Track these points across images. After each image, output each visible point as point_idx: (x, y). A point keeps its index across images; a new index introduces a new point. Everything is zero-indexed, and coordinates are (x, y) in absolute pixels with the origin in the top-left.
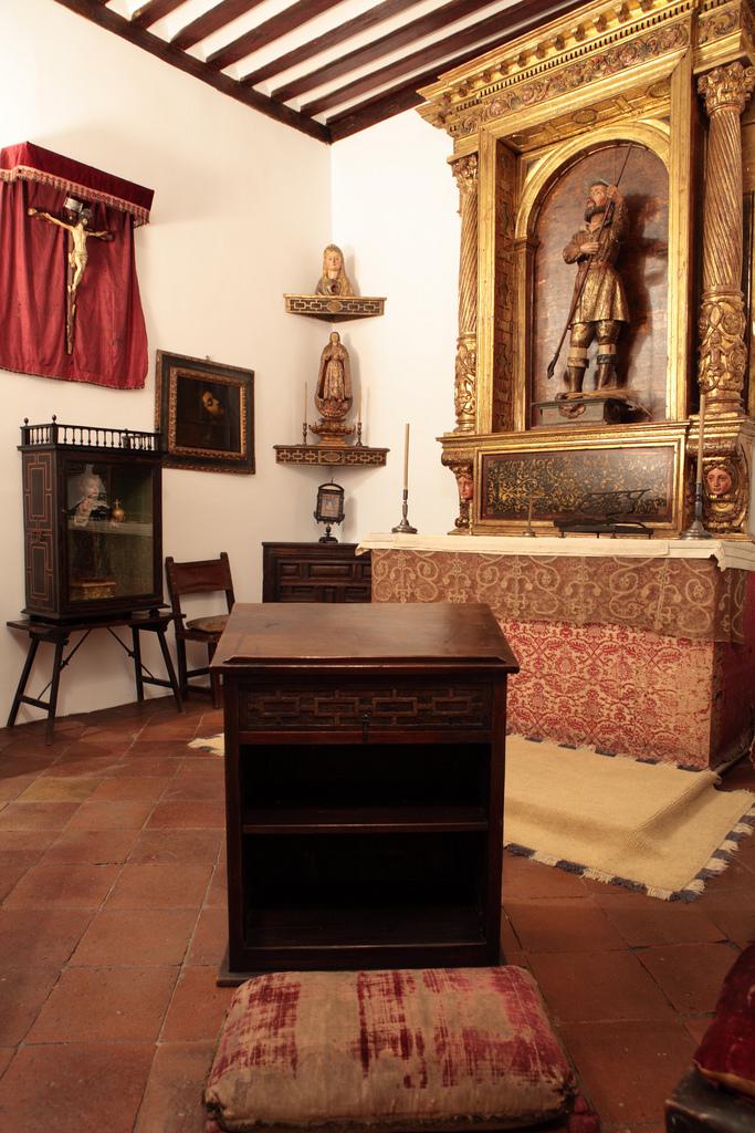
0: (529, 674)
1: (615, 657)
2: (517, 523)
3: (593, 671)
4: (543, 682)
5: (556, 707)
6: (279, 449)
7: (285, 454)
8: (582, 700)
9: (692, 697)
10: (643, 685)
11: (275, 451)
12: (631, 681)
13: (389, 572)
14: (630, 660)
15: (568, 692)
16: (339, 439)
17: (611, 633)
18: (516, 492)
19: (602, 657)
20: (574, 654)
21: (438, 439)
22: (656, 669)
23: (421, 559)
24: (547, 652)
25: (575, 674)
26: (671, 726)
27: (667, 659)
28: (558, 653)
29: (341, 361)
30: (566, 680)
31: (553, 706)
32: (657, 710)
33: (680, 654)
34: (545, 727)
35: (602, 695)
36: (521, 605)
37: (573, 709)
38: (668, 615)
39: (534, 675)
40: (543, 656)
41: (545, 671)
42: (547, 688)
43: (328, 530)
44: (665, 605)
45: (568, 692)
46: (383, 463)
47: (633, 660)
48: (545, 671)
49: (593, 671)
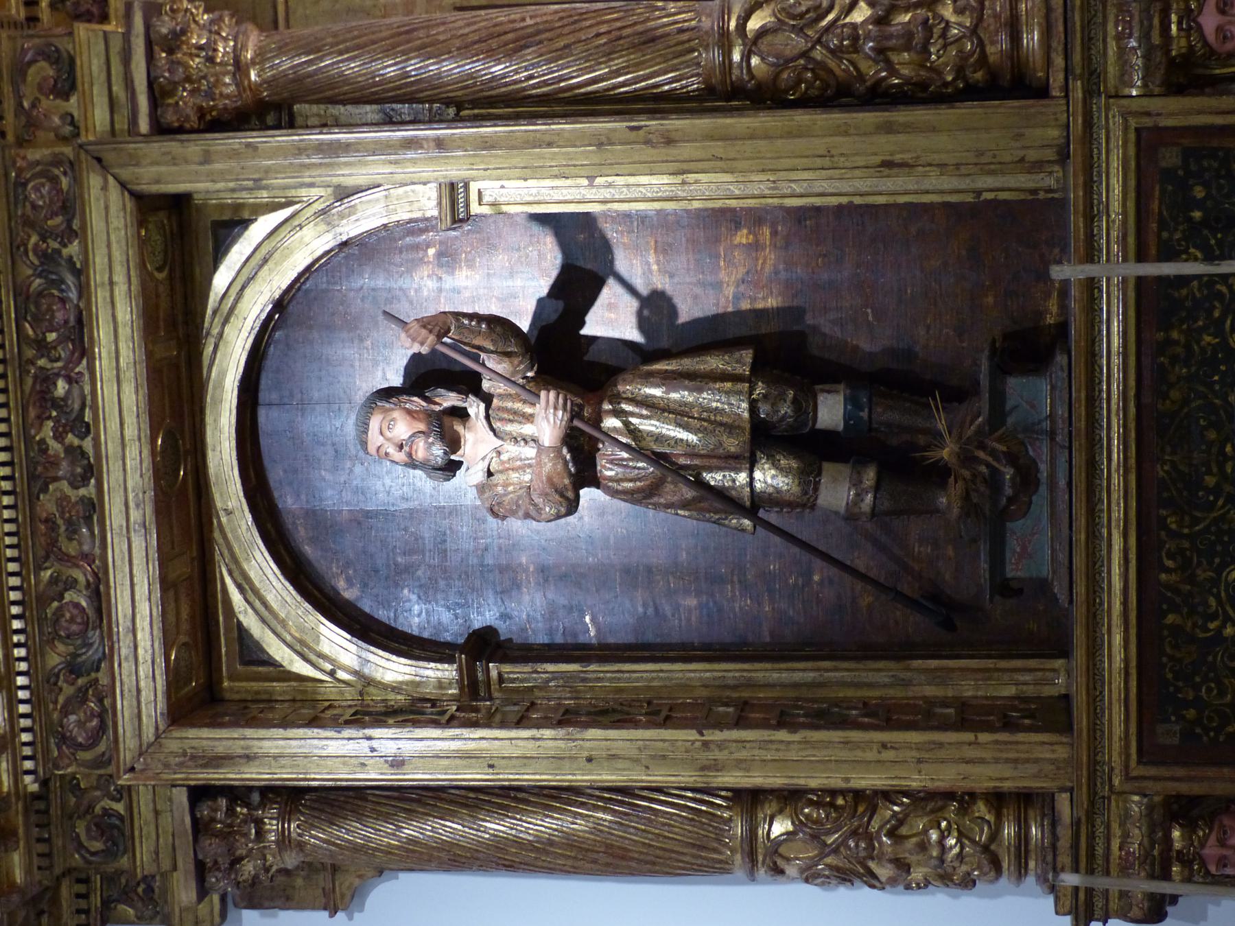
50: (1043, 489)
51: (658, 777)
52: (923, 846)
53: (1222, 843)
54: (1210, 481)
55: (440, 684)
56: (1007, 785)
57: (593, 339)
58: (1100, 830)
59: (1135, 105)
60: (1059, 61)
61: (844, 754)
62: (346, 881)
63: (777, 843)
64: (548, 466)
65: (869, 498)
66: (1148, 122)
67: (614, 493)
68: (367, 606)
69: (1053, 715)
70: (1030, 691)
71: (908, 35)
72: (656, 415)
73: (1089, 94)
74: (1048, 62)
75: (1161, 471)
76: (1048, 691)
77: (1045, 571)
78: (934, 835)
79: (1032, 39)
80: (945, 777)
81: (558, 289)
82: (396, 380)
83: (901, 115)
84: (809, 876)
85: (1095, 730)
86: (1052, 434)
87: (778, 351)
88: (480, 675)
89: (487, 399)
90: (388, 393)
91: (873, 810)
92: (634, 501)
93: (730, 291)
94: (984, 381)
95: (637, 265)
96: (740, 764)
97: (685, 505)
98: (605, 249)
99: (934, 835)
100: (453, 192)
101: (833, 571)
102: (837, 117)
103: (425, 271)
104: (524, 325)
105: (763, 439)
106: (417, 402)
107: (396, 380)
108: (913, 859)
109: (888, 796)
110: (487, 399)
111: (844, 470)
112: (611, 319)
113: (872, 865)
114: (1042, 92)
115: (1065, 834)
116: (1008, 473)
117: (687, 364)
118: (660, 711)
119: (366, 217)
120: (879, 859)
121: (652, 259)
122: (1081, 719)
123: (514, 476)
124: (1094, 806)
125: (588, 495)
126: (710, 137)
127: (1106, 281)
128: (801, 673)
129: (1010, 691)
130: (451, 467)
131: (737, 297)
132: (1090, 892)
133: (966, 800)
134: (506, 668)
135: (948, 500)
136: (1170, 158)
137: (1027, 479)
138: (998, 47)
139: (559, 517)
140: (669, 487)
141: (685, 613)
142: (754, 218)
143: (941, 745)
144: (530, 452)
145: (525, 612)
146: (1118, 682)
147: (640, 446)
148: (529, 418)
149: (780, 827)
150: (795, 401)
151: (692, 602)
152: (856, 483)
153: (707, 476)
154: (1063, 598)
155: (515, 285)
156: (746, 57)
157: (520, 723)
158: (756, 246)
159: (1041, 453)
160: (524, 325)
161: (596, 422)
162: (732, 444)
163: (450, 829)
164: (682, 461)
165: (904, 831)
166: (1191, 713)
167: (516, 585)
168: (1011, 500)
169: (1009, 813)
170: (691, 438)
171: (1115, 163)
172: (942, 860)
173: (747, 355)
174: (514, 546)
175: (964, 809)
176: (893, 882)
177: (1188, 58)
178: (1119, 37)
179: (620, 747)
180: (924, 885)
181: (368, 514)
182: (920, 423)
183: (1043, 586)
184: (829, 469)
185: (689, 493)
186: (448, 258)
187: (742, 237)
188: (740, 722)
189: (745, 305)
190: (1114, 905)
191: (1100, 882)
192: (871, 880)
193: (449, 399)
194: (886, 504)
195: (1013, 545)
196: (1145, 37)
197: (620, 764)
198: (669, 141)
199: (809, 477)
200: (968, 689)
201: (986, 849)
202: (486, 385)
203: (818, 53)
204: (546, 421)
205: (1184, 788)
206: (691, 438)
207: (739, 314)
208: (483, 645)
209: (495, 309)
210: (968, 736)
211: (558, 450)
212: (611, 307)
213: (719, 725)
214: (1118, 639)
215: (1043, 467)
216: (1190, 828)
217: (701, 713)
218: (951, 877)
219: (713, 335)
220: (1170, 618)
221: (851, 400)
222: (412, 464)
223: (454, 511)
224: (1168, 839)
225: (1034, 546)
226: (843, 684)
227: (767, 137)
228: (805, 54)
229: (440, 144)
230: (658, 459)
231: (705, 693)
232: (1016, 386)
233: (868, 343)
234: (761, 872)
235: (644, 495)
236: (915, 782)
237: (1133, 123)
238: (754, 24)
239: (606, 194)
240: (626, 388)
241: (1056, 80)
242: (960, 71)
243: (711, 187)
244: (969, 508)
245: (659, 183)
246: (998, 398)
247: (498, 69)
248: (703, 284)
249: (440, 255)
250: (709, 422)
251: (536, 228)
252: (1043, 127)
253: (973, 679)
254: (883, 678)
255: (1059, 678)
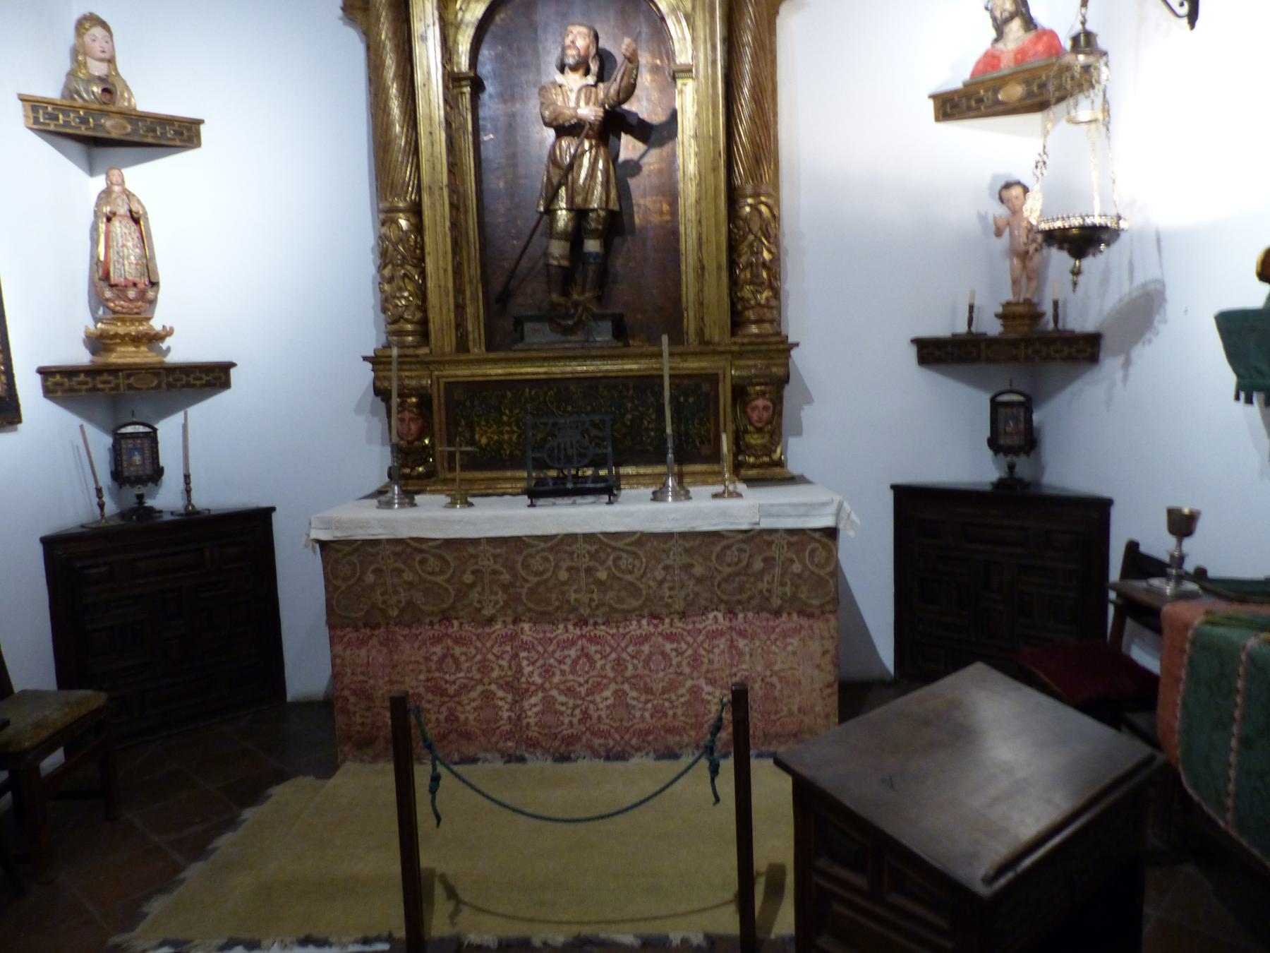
0: (472, 683)
1: (722, 643)
2: (509, 474)
3: (695, 661)
4: (626, 687)
5: (647, 714)
6: (45, 372)
7: (59, 382)
8: (682, 700)
9: (816, 672)
10: (759, 668)
11: (38, 378)
12: (744, 667)
13: (363, 573)
14: (741, 643)
15: (663, 692)
16: (143, 349)
17: (715, 620)
18: (502, 433)
19: (706, 645)
20: (668, 647)
21: (365, 359)
22: (774, 648)
23: (421, 551)
24: (630, 649)
25: (595, 673)
26: (795, 709)
27: (785, 635)
28: (646, 649)
29: (135, 219)
30: (658, 679)
31: (642, 714)
32: (777, 694)
33: (801, 627)
34: (634, 741)
35: (709, 688)
36: (591, 600)
37: (670, 713)
38: (788, 589)
39: (481, 682)
40: (625, 655)
41: (629, 673)
42: (634, 694)
43: (140, 498)
44: (783, 575)
45: (663, 692)
46: (226, 384)
47: (746, 641)
48: (629, 673)
49: (695, 661)
50: (563, 338)
51: (425, 166)
52: (400, 289)
53: (411, 419)
54: (569, 408)
55: (459, 64)
56: (431, 325)
57: (619, 139)
58: (413, 367)
59: (728, 373)
60: (746, 340)
61: (440, 253)
62: (359, 16)
63: (397, 223)
64: (568, 112)
65: (555, 263)
66: (721, 377)
67: (553, 147)
68: (492, 28)
69: (462, 345)
70: (471, 337)
71: (759, 276)
72: (589, 163)
73: (732, 353)
74: (745, 336)
75: (573, 388)
76: (471, 344)
77: (527, 340)
78: (406, 294)
79: (754, 329)
80: (433, 298)
81: (642, 122)
82: (602, 44)
83: (725, 274)
84: (382, 238)
85: (458, 363)
86: (587, 341)
87: (616, 224)
88: (464, 83)
89: (595, 85)
90: (596, 37)
91: (415, 266)
92: (549, 157)
93: (642, 202)
94: (609, 311)
95: (653, 159)
96: (433, 205)
97: (549, 179)
98: (660, 143)
99: (406, 294)
100: (687, 71)
101: (519, 251)
102: (724, 245)
103: (650, 59)
104: (626, 107)
105: (580, 214)
106: (593, 51)
107: (602, 44)
108: (394, 284)
109: (423, 273)
110: (595, 85)
111: (567, 251)
112: (629, 147)
113: (390, 267)
114: (733, 334)
115: (411, 351)
116: (570, 322)
117: (613, 180)
118: (454, 167)
119: (677, 30)
120: (393, 270)
121: (656, 166)
122: (462, 357)
123: (560, 98)
124: (425, 364)
125: (550, 133)
126: (716, 189)
127: (666, 363)
128: (473, 234)
129: (470, 328)
130: (562, 71)
131: (639, 205)
132: (390, 363)
133: (423, 308)
134: (468, 96)
135: (555, 297)
136: (706, 387)
137: (567, 331)
138: (751, 315)
139: (543, 118)
140: (557, 171)
141: (495, 183)
142: (674, 212)
143: (447, 296)
144: (572, 104)
145: (491, 105)
146: (480, 372)
147: (576, 158)
148: (587, 103)
149: (403, 223)
150: (597, 230)
151: (501, 185)
152: (562, 257)
153: (563, 189)
154: (516, 347)
155: (642, 106)
156: (750, 205)
157: (446, 101)
158: (661, 213)
159: (579, 337)
160: (626, 107)
161: (587, 137)
162: (579, 200)
163: (390, 61)
164: (570, 177)
165: (407, 280)
166: (468, 404)
167: (505, 102)
168: (559, 325)
169: (418, 328)
170: (581, 181)
171: (704, 364)
172: (395, 297)
173: (616, 208)
174: (523, 100)
175: (418, 307)
176: (382, 276)
177: (747, 394)
178: (755, 366)
179: (437, 147)
180: (382, 291)
181: (535, 31)
182: (587, 287)
183: (522, 338)
184: (567, 245)
185: (555, 181)
186: (655, 70)
187: (666, 207)
188: (452, 205)
189: (635, 209)
190: (381, 374)
191: (394, 366)
192: (381, 268)
193: (594, 67)
194: (553, 271)
195: (538, 326)
196: (756, 376)
197: (429, 147)
198: (715, 169)
199: (564, 236)
200: (470, 310)
201: (401, 317)
202: (601, 85)
203: (751, 237)
204: (589, 112)
205: (435, 402)
206: (581, 181)
207: (632, 206)
208: (477, 86)
209: (637, 92)
210: (452, 307)
211: (576, 116)
212: (634, 148)
213: (450, 196)
214: (500, 371)
215: (573, 338)
216: (417, 405)
217: (455, 188)
218: (386, 303)
219: (624, 194)
220: (509, 394)
221: (597, 255)
222: (564, 49)
223: (539, 72)
224: (411, 396)
225: (538, 334)
226: (469, 254)
227: (716, 214)
228: (751, 231)
229: (714, 62)
230: (571, 166)
231: (461, 191)
232: (607, 325)
233: (619, 263)
234: (382, 216)
235: (553, 160)
236: (431, 284)
237: (720, 372)
238: (763, 208)
239: (686, 143)
240: (602, 151)
241: (738, 340)
242: (742, 299)
243: (689, 191)
244: (555, 306)
245: (692, 168)
246: (602, 317)
247: (746, 90)
248: (645, 190)
249: (657, 66)
250: (588, 190)
251: (669, 112)
252: (717, 333)
253: (474, 311)
254: (473, 271)
255: (477, 350)
